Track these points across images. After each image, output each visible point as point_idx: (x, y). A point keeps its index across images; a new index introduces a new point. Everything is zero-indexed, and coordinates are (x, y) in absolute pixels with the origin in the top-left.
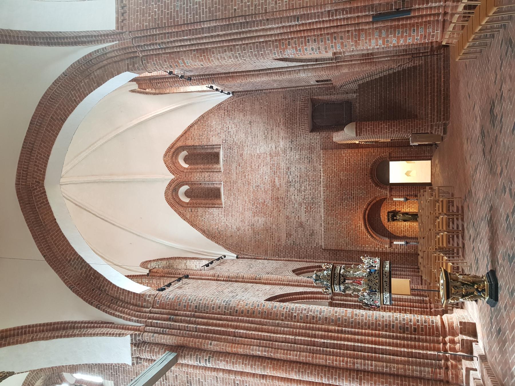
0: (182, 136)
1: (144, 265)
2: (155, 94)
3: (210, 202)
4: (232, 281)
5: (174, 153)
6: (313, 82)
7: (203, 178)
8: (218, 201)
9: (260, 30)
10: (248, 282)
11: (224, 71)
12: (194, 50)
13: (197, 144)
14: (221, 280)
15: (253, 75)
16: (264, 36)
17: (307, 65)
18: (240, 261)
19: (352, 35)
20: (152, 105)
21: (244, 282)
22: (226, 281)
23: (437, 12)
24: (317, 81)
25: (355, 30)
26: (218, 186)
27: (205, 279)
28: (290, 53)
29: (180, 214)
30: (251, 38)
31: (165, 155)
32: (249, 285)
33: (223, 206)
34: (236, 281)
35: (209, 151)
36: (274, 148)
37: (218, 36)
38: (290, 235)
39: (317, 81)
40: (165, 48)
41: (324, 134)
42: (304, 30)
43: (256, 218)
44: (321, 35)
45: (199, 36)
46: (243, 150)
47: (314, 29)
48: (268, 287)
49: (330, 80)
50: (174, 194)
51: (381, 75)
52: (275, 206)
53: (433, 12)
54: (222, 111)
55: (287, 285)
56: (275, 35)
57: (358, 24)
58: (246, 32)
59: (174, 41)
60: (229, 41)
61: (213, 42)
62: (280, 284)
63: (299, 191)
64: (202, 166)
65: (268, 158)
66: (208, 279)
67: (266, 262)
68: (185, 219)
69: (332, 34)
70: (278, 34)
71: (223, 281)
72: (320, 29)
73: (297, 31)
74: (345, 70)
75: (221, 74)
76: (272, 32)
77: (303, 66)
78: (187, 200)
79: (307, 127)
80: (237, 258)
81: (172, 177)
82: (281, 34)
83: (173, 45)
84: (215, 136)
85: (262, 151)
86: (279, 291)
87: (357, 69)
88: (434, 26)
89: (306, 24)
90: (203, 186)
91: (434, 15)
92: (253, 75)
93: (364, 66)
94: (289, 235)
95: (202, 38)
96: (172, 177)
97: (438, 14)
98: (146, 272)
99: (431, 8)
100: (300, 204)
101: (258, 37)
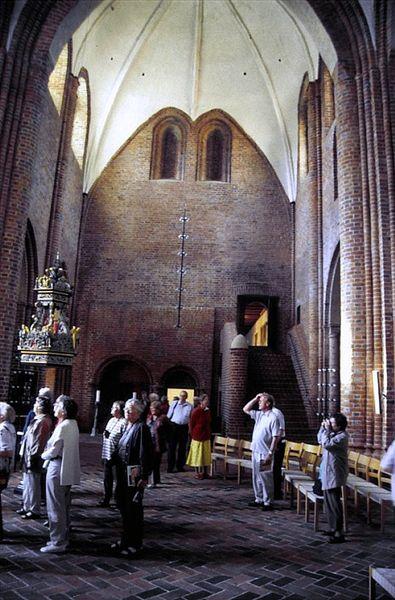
0: (245, 135)
1: (84, 73)
2: (302, 88)
3: (158, 164)
4: (55, 181)
5: (221, 121)
6: (299, 302)
7: (190, 158)
8: (158, 175)
9: (377, 229)
10: (53, 202)
11: (324, 189)
12: (359, 145)
13: (233, 152)
14: (57, 167)
15: (317, 225)
16: (369, 234)
17: (322, 293)
18: (80, 197)
19: (362, 342)
20: (286, 92)
21: (53, 198)
22: (56, 173)
23: (376, 440)
24: (299, 307)
25: (365, 346)
26: (177, 177)
27: (60, 147)
28: (346, 265)
29: (146, 124)
30: (369, 213)
31: (222, 112)
32: (49, 203)
33: (152, 181)
34: (55, 187)
35: (224, 167)
36: (222, 249)
37: (375, 176)
38: (109, 264)
39: (299, 307)
40: (363, 108)
41: (234, 312)
42: (372, 283)
43: (133, 221)
44: (365, 305)
45: (376, 152)
46: (222, 211)
47: (372, 296)
48: (45, 226)
49: (299, 322)
50: (171, 119)
51: (300, 382)
52: (147, 246)
53: (375, 436)
54: (273, 189)
55: (47, 251)
56: (370, 247)
57: (373, 350)
58: (376, 212)
59: (371, 121)
60: (367, 189)
61: (367, 170)
62: (48, 240)
63: (165, 278)
64: (204, 157)
65: (209, 242)
66: (60, 151)
67: (77, 230)
68: (139, 131)
69: (364, 318)
70: (370, 251)
71: (57, 170)
72: (372, 304)
73: (371, 275)
74: (311, 339)
75: (321, 185)
76: (373, 244)
77: (322, 288)
78: (283, 441)
79: (242, 293)
80: (84, 194)
81: (194, 118)
82: (370, 255)
83: (367, 120)
84: (240, 173)
85: (219, 235)
86: (41, 238)
87: (311, 352)
88: (359, 437)
89: (380, 286)
90: (179, 155)
91: (372, 438)
92: (317, 225)
93: (315, 361)
94: (109, 262)
95: (373, 156)
96: (194, 118)
97: (372, 442)
98: (76, 73)
99: (381, 434)
100: (148, 278)
101: (369, 226)
